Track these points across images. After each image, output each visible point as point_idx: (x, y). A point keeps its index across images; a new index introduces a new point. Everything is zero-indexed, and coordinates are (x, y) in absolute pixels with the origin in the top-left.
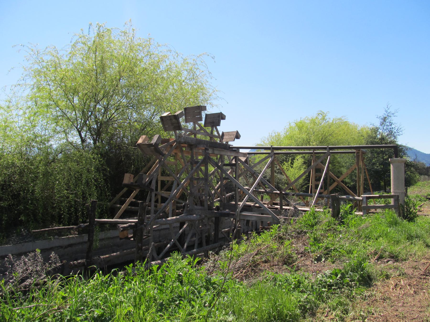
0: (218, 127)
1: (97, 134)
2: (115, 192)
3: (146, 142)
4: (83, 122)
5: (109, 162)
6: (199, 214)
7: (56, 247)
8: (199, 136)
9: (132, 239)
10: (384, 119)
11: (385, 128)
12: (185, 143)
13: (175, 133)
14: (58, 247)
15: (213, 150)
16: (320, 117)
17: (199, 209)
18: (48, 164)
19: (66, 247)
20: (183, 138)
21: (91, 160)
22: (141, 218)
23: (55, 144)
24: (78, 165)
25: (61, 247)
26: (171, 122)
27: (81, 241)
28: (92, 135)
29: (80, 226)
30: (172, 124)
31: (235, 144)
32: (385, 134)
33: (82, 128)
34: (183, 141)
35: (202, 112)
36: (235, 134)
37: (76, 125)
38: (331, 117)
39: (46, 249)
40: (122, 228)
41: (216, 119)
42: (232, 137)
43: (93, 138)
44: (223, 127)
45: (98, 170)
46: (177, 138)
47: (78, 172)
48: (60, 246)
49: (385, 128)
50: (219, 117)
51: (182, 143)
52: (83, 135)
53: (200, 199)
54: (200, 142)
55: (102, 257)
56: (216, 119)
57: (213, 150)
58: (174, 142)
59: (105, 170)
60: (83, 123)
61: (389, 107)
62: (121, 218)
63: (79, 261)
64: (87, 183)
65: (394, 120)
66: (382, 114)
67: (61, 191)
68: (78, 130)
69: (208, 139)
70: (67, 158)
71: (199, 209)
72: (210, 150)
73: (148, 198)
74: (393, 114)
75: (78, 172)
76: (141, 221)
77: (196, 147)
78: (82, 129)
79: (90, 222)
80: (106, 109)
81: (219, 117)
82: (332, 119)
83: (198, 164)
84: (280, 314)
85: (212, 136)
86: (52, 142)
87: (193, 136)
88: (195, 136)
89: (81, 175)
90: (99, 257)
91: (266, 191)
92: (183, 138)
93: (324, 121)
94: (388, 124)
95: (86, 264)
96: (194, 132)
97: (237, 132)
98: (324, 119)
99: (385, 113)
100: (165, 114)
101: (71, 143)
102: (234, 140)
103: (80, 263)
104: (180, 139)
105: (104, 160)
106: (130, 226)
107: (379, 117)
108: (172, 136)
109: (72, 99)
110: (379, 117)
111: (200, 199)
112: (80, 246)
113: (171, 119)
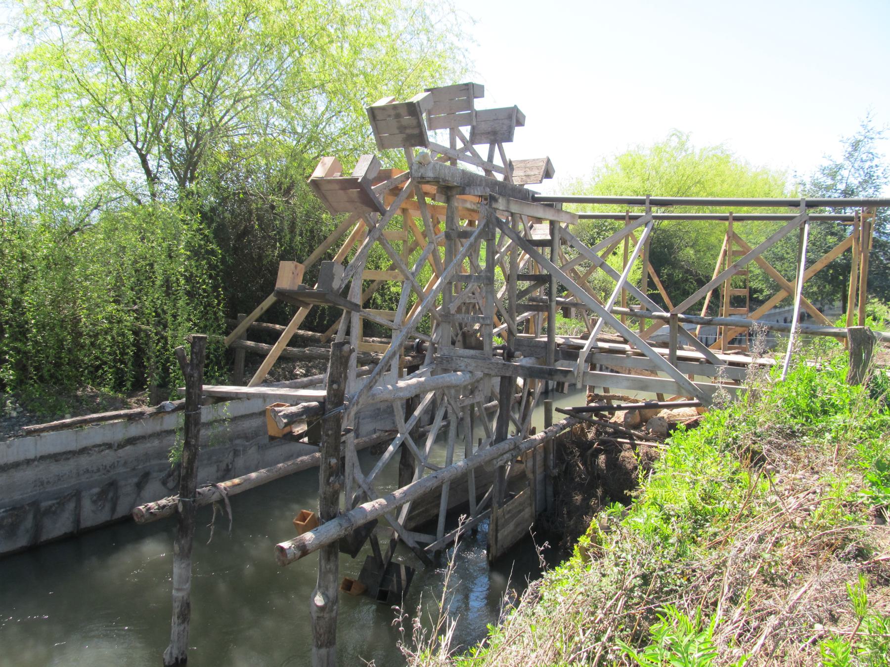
0: (504, 145)
1: (188, 165)
2: (237, 307)
3: (337, 176)
4: (151, 130)
5: (220, 234)
6: (470, 368)
7: (95, 446)
8: (463, 165)
9: (306, 439)
10: (856, 146)
11: (856, 165)
12: (436, 181)
13: (408, 155)
14: (100, 446)
15: (508, 201)
16: (674, 142)
17: (468, 357)
18: (68, 234)
19: (121, 446)
20: (431, 166)
21: (177, 228)
22: (335, 386)
23: (82, 185)
24: (143, 239)
25: (109, 446)
26: (401, 123)
27: (158, 428)
28: (172, 167)
29: (163, 407)
30: (402, 128)
31: (545, 189)
32: (854, 182)
33: (149, 144)
34: (430, 174)
35: (475, 100)
36: (543, 165)
37: (133, 137)
38: (700, 142)
39: (70, 452)
40: (285, 416)
41: (502, 125)
42: (536, 172)
43: (178, 173)
44: (520, 148)
45: (196, 253)
46: (415, 167)
47: (145, 258)
48: (104, 444)
49: (856, 165)
50: (510, 117)
51: (428, 182)
52: (152, 164)
53: (461, 329)
54: (469, 181)
55: (222, 485)
56: (502, 125)
57: (508, 201)
58: (407, 176)
59: (213, 252)
60: (152, 135)
61: (870, 116)
62: (265, 383)
63: (163, 502)
64: (167, 283)
65: (878, 146)
66: (853, 132)
67: (99, 309)
68: (139, 151)
69: (481, 172)
70: (113, 225)
71: (468, 357)
72: (500, 200)
73: (341, 325)
74: (879, 133)
75: (145, 258)
76: (336, 397)
77: (463, 193)
78: (148, 152)
79: (188, 394)
80: (209, 102)
81: (510, 117)
82: (697, 151)
83: (472, 239)
84: (572, 556)
85: (489, 167)
86: (73, 179)
87: (448, 163)
88: (454, 163)
89: (151, 265)
90: (214, 486)
91: (631, 310)
92: (431, 166)
93: (684, 154)
94: (864, 157)
95: (180, 509)
96: (451, 156)
97: (548, 161)
98: (682, 146)
99: (861, 129)
100: (382, 102)
101: (121, 186)
102: (541, 182)
103: (164, 506)
104: (422, 171)
105: (209, 228)
106: (307, 410)
107: (845, 139)
108: (396, 160)
109: (119, 68)
110: (845, 139)
111: (461, 329)
112: (156, 443)
113: (398, 116)
